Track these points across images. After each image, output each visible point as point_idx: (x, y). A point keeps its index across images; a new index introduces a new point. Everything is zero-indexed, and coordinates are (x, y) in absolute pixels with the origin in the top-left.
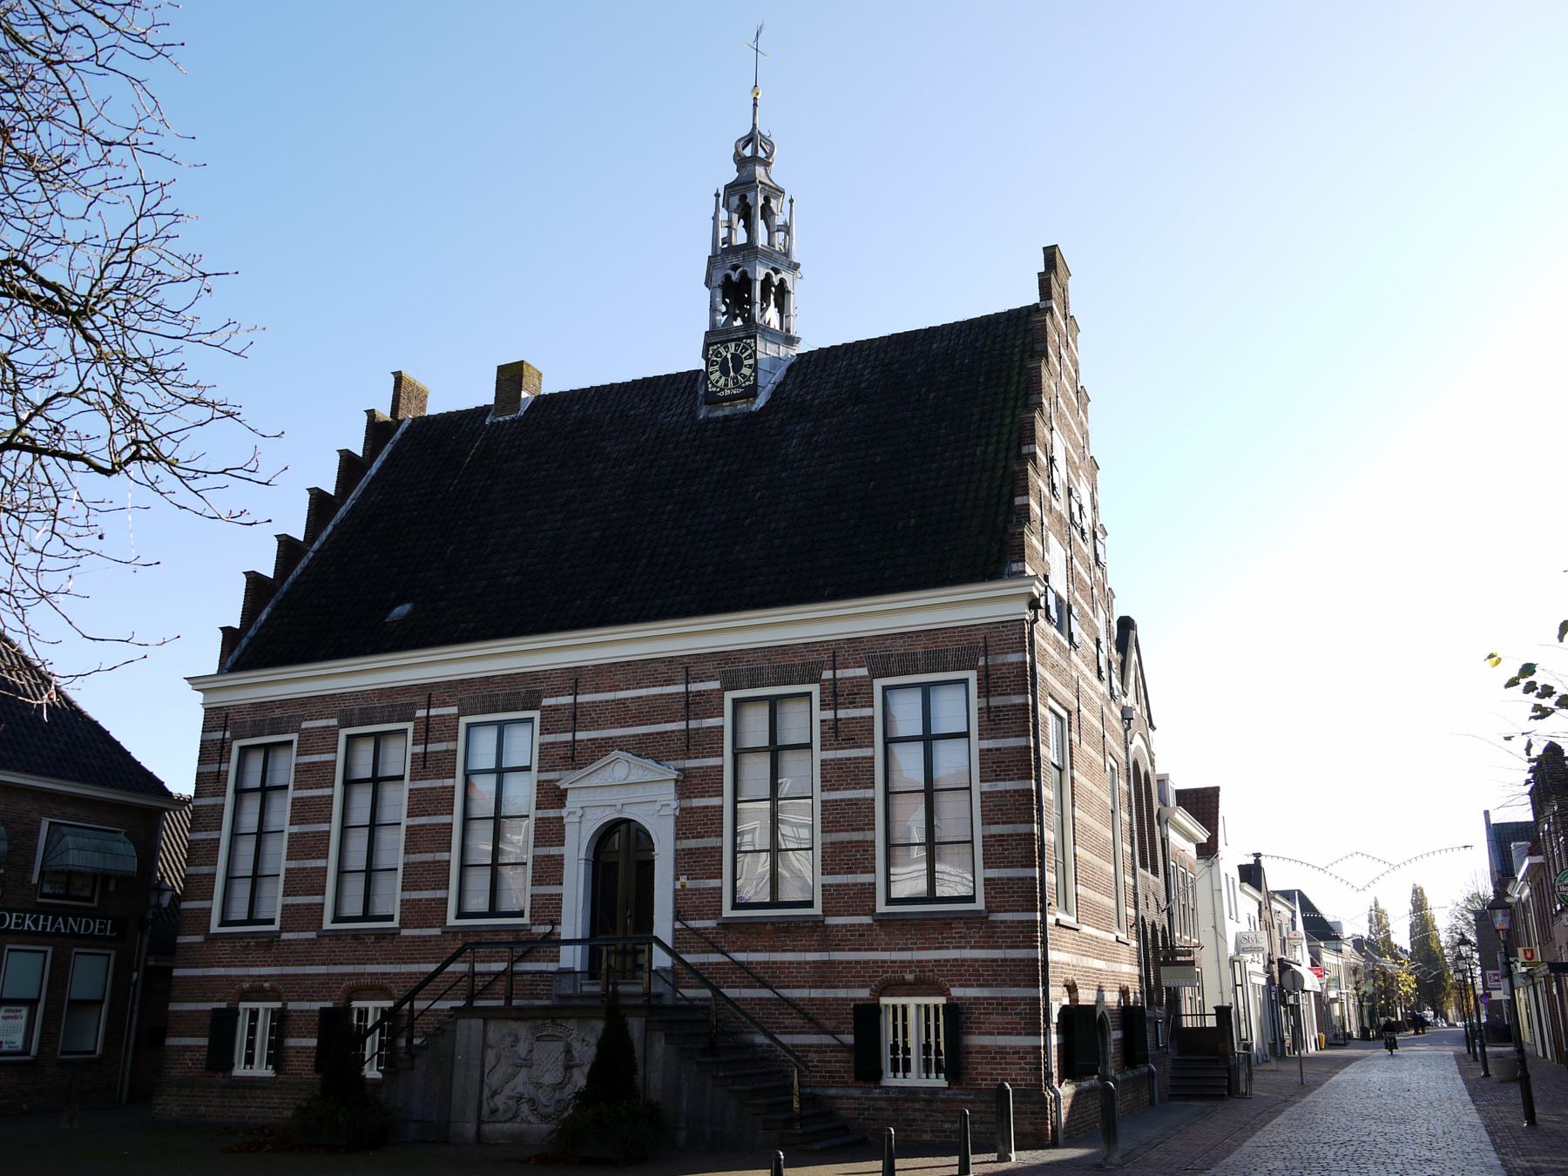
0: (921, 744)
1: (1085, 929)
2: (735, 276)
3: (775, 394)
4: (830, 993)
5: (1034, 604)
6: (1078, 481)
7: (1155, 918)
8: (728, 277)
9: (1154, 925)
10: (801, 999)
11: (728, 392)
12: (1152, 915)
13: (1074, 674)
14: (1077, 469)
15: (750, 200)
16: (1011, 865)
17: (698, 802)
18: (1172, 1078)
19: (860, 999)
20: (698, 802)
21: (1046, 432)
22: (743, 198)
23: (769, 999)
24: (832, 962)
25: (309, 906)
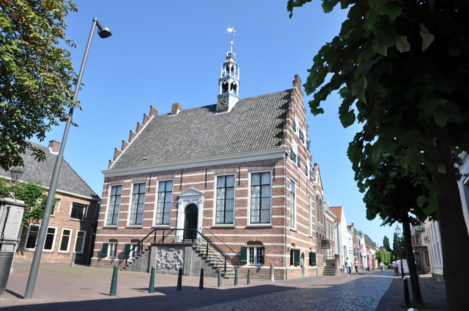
0: (259, 187)
1: (298, 232)
2: (225, 83)
3: (233, 109)
4: (236, 244)
5: (287, 155)
6: (302, 129)
7: (321, 233)
8: (223, 83)
9: (320, 235)
10: (229, 245)
11: (222, 108)
12: (320, 232)
13: (299, 173)
14: (302, 126)
15: (229, 66)
16: (278, 215)
17: (208, 200)
18: (324, 271)
19: (242, 245)
20: (208, 200)
21: (293, 116)
22: (227, 66)
23: (222, 245)
24: (236, 237)
25: (124, 221)
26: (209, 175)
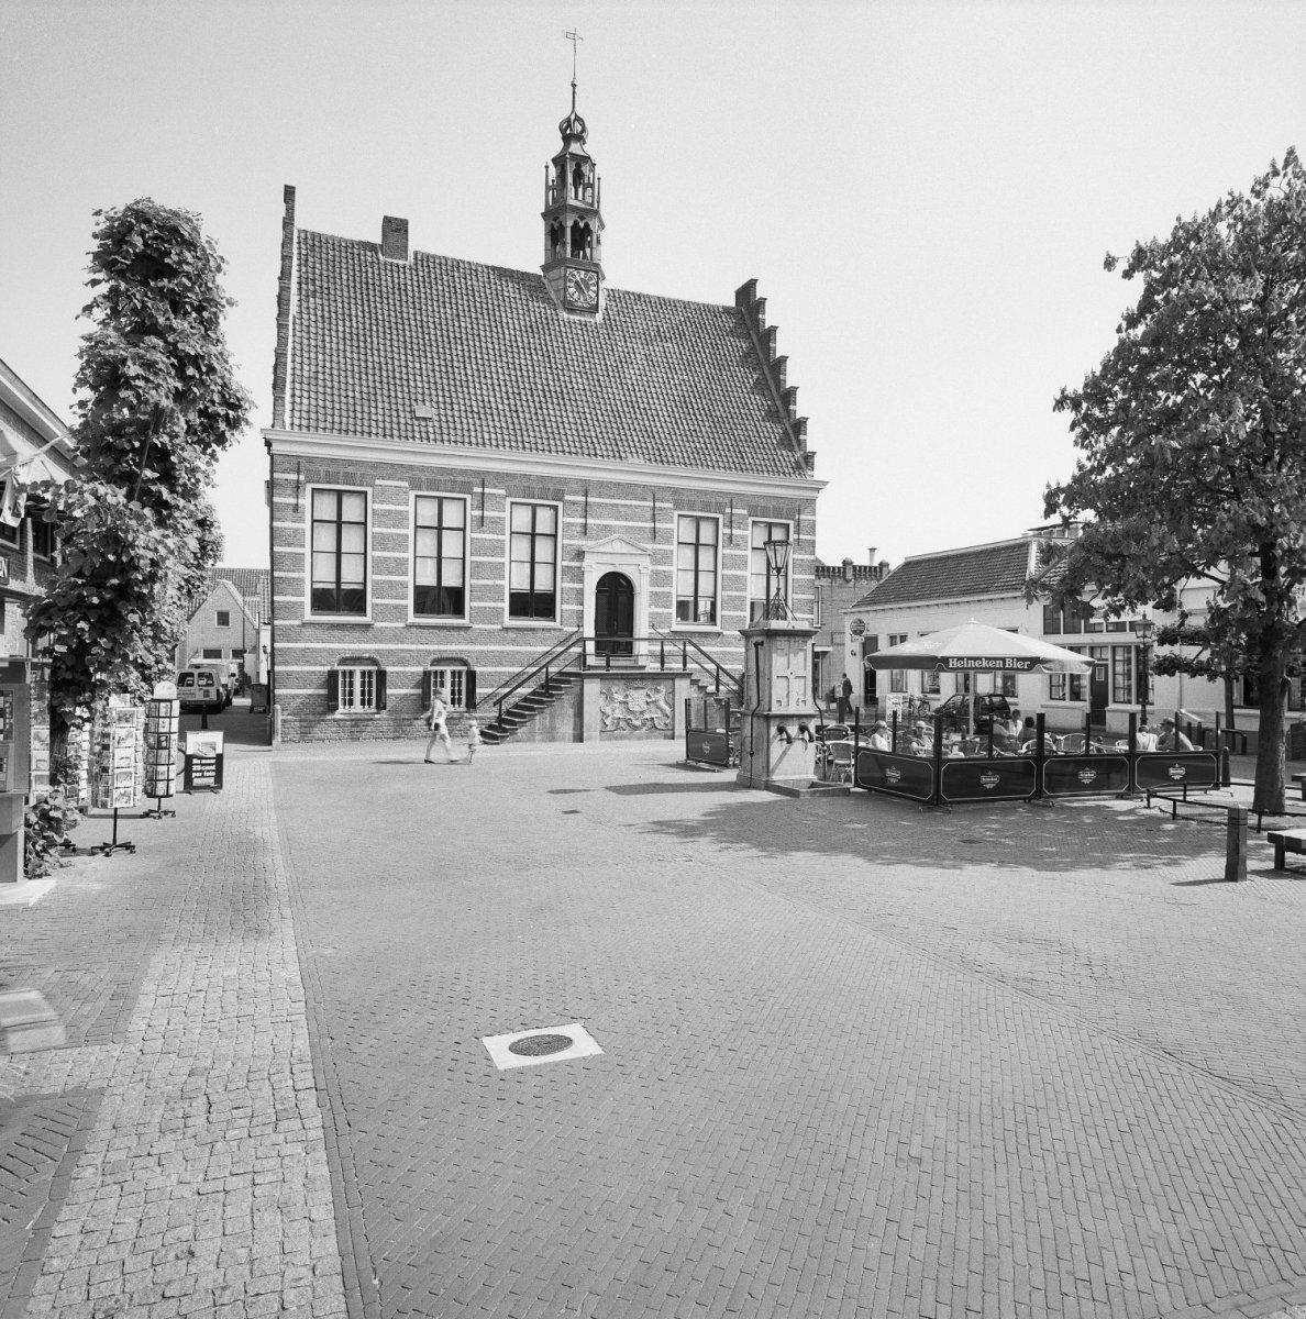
17: (660, 568)
20: (660, 568)
26: (661, 509)
